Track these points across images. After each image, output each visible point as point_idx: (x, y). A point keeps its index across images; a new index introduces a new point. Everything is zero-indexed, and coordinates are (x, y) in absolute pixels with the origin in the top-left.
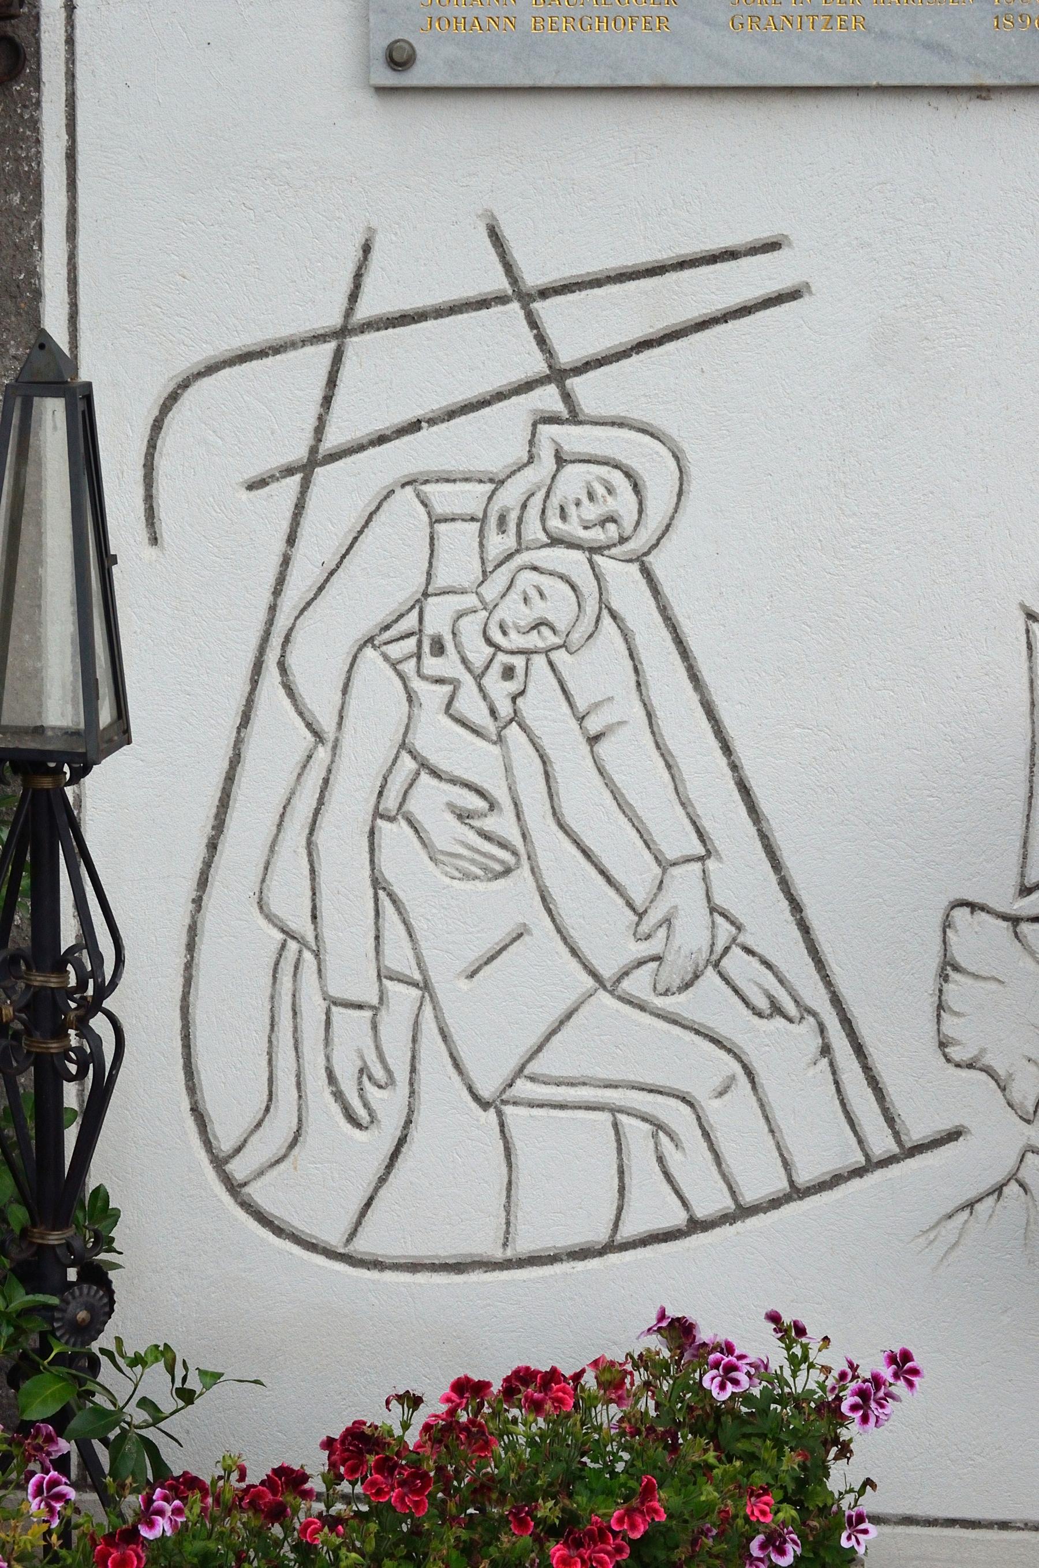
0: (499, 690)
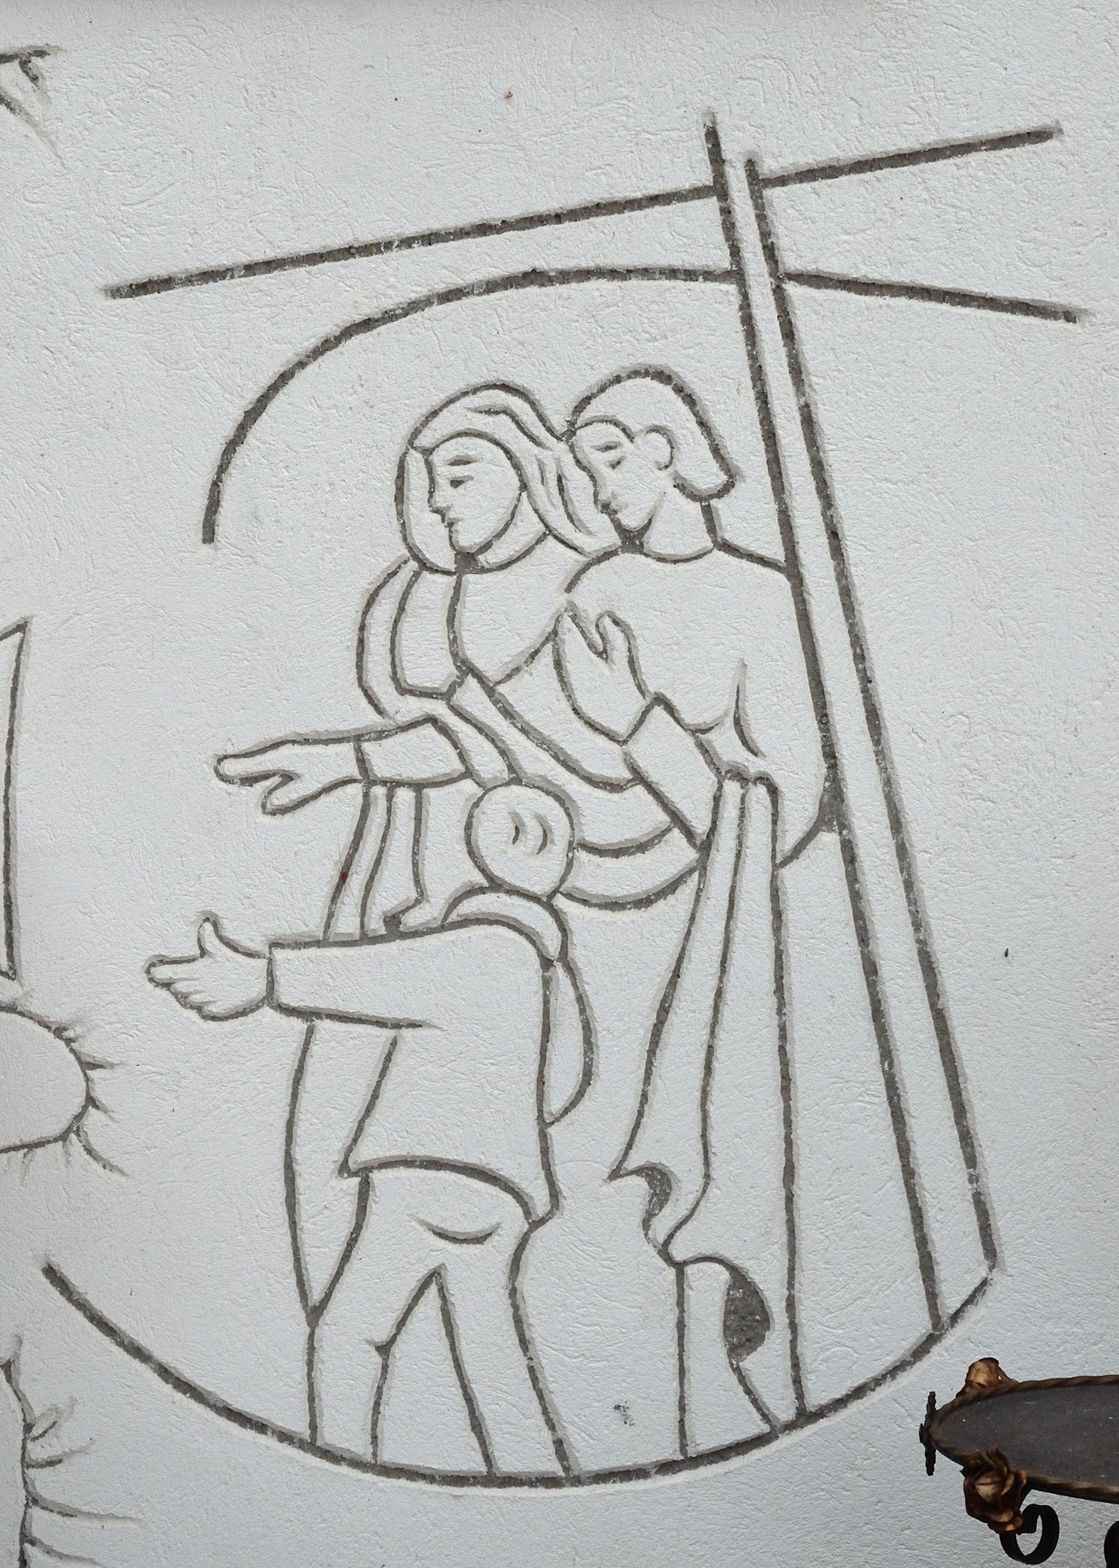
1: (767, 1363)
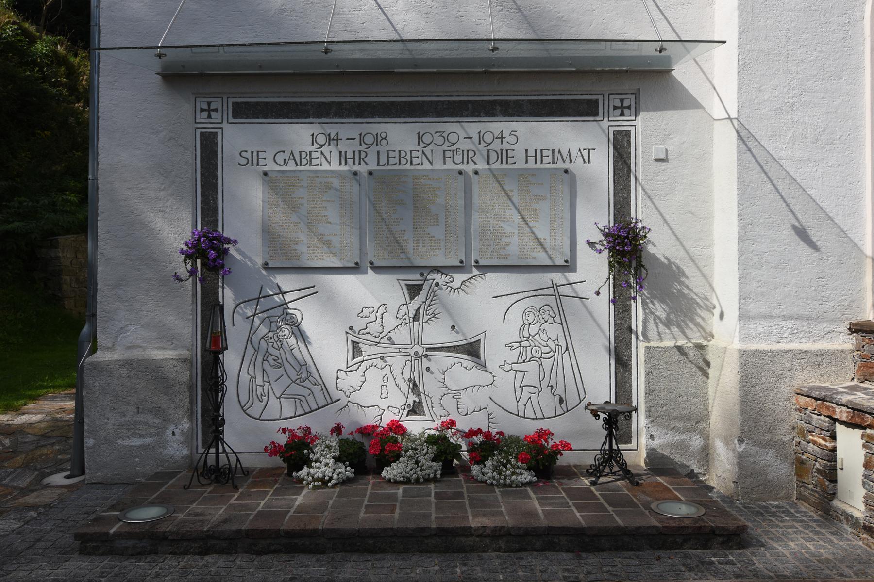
0: (279, 344)
1: (563, 405)
